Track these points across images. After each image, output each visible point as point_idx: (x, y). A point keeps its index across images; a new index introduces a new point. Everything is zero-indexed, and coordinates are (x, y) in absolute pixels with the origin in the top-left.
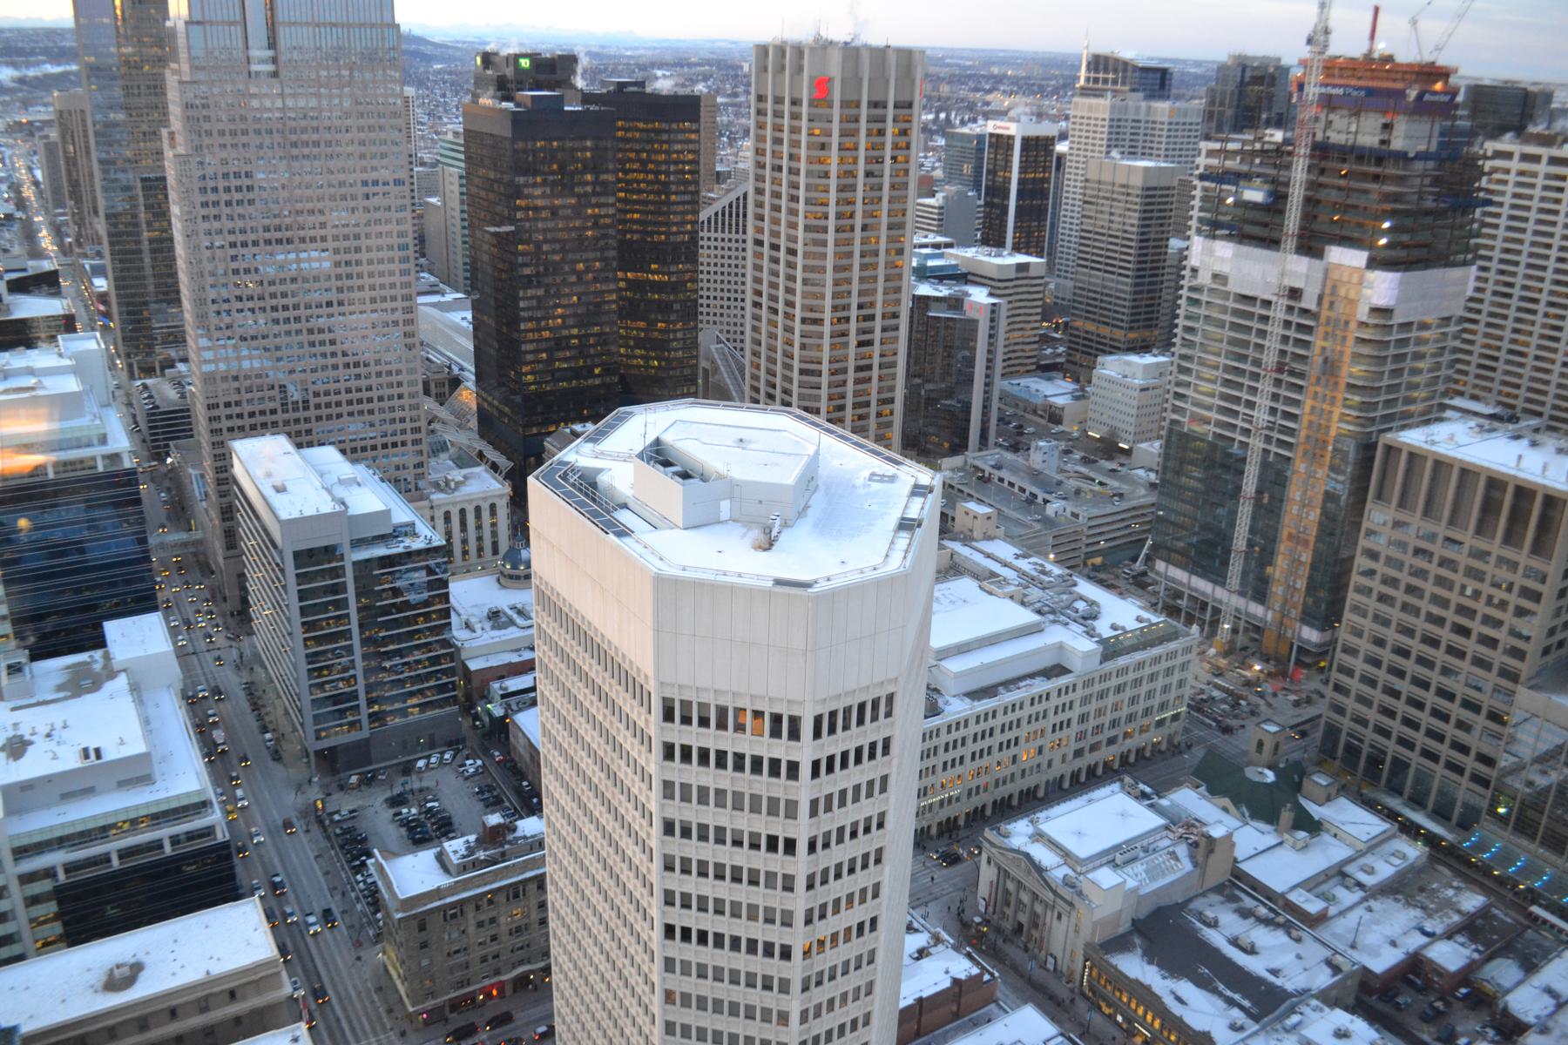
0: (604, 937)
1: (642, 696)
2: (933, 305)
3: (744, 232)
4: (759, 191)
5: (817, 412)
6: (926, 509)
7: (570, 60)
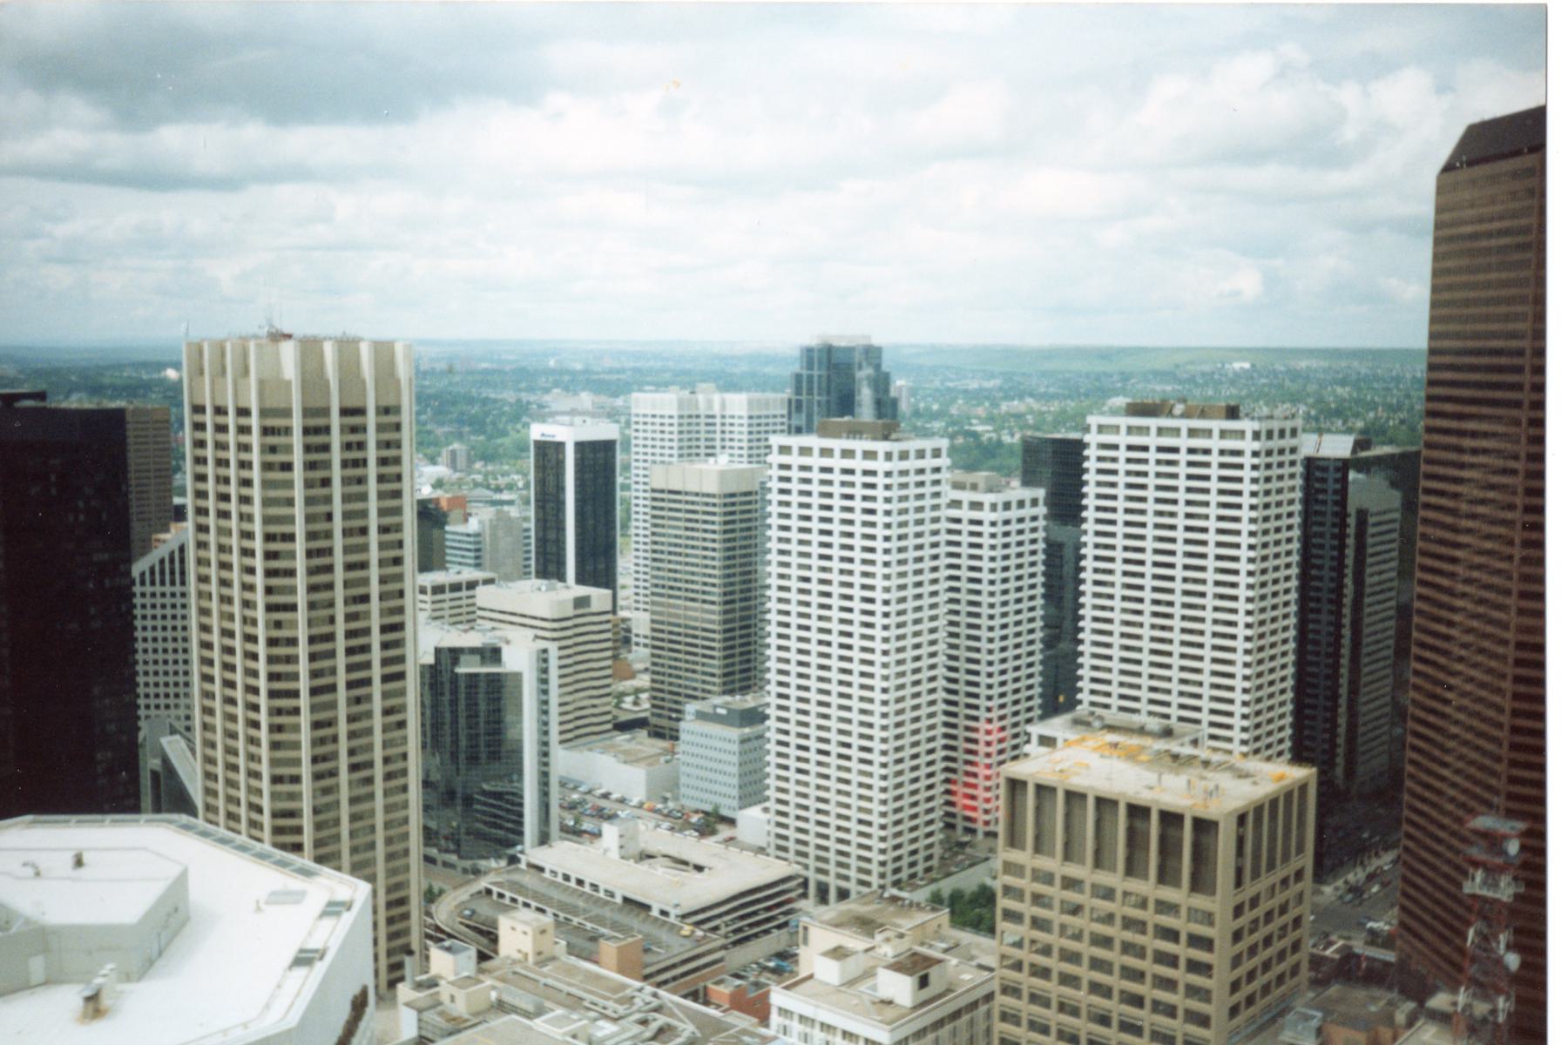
2: (463, 658)
3: (183, 583)
4: (201, 545)
5: (297, 848)
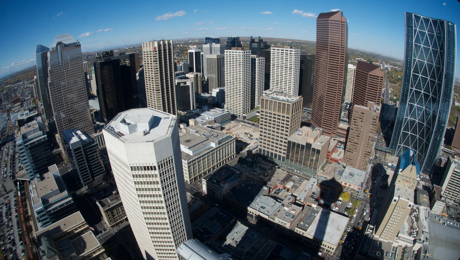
0: (133, 210)
1: (127, 166)
6: (173, 123)
7: (112, 52)
